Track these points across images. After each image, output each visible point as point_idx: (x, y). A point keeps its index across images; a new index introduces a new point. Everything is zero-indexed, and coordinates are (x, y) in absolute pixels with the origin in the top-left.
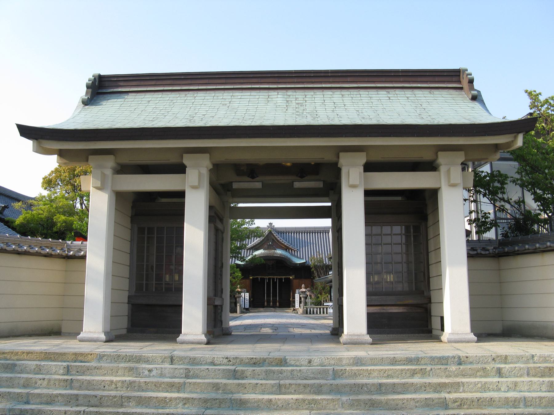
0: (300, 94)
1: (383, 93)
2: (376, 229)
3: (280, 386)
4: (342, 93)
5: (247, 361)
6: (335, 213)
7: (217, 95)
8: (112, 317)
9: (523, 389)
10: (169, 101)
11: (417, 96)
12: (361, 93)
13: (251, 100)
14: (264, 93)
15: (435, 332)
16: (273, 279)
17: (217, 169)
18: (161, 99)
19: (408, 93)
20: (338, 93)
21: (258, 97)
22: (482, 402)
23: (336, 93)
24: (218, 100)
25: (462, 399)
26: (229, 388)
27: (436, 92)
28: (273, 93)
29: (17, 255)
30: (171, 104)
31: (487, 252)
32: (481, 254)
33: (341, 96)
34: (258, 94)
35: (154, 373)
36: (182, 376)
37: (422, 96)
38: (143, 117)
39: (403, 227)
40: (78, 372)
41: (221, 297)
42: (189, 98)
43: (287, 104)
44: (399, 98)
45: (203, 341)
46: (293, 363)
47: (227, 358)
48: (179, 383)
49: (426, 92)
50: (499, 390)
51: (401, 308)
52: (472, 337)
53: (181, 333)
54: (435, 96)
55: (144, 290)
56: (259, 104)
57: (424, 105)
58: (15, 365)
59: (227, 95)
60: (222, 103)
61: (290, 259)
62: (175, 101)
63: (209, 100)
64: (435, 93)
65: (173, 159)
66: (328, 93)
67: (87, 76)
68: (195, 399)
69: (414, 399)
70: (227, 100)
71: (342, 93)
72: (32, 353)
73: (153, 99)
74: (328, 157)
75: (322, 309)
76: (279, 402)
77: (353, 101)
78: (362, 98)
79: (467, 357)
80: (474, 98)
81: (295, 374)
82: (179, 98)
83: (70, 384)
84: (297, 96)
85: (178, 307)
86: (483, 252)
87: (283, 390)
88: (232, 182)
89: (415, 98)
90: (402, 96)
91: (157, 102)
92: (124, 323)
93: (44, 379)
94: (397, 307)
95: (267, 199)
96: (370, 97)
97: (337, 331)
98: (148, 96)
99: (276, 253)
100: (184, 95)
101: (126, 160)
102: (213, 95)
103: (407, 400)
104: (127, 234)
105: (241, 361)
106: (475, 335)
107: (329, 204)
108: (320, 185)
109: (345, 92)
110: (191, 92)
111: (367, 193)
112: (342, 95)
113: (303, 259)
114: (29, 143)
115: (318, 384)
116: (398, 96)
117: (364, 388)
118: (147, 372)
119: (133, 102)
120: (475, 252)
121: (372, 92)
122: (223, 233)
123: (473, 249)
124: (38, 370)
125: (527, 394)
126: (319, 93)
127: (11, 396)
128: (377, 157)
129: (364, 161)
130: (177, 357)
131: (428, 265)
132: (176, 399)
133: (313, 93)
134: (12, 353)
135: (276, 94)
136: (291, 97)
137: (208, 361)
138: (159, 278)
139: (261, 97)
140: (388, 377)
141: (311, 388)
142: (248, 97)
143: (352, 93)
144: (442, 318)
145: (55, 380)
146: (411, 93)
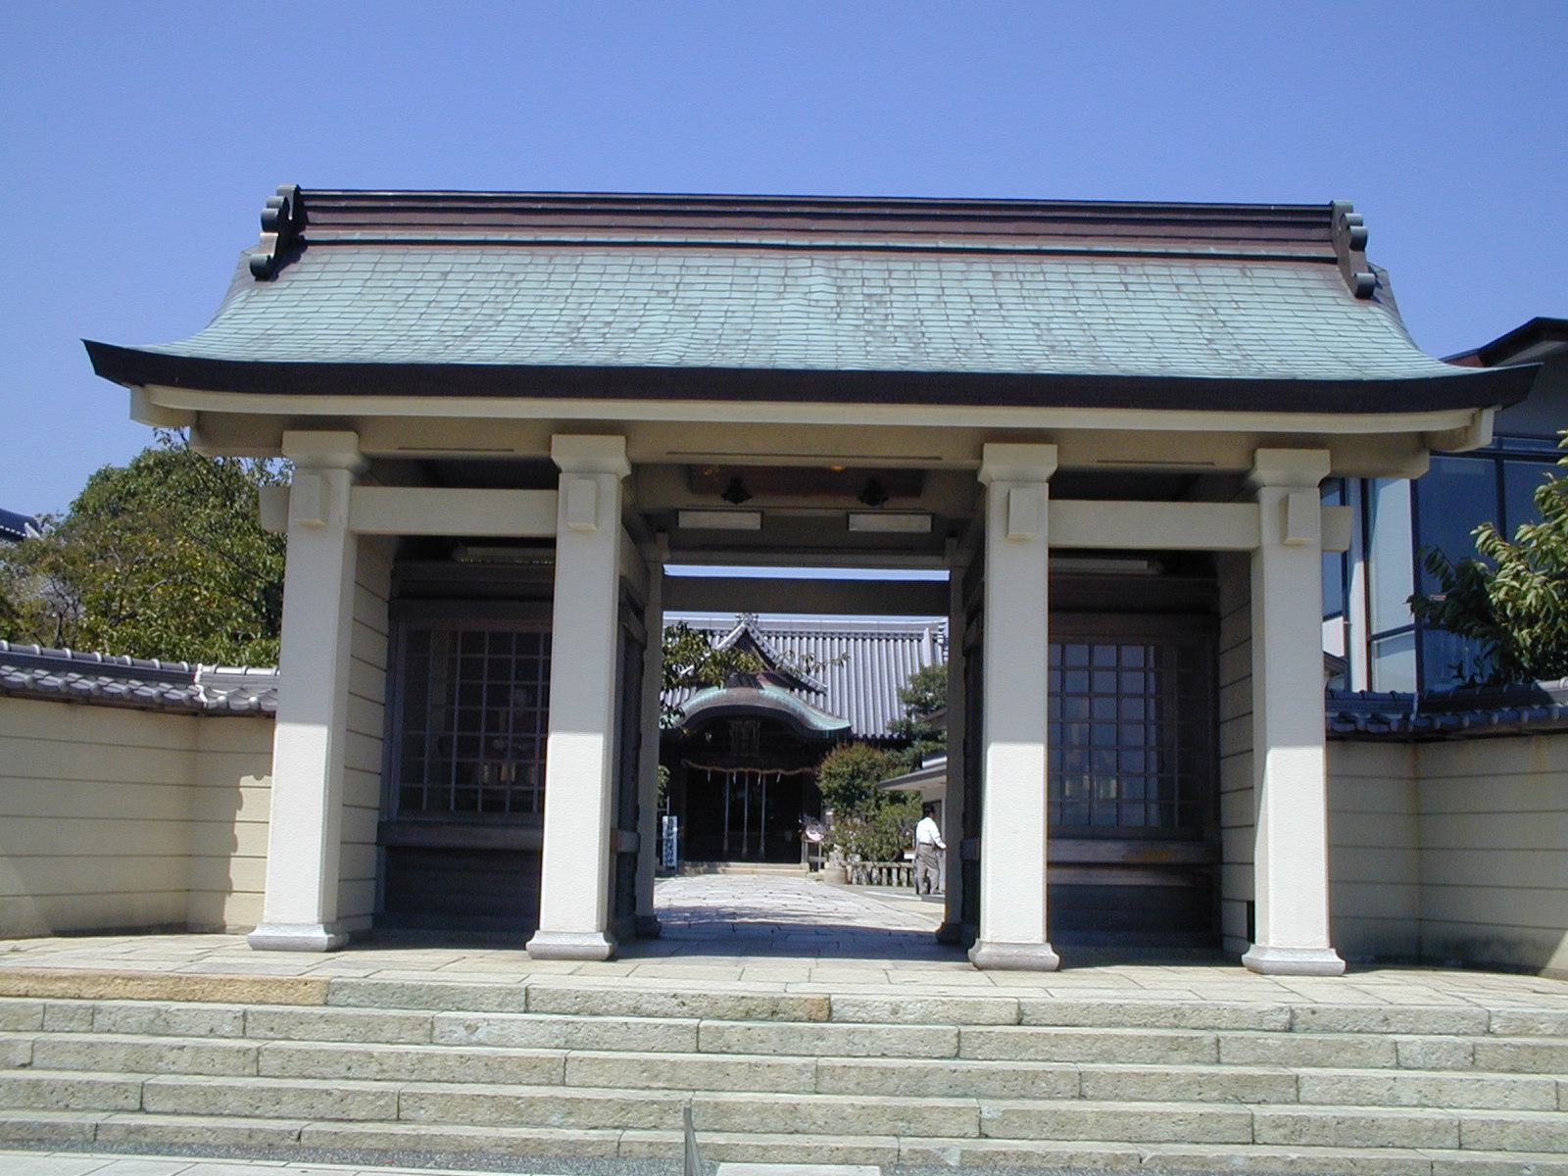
0: (872, 268)
1: (1108, 269)
2: (1077, 654)
3: (818, 1071)
4: (995, 268)
5: (730, 1004)
6: (965, 605)
7: (639, 261)
8: (342, 882)
9: (1459, 1100)
10: (502, 277)
11: (1204, 281)
12: (1046, 268)
13: (737, 280)
14: (773, 262)
15: (1229, 945)
16: (753, 777)
17: (639, 475)
18: (480, 268)
19: (1181, 271)
20: (981, 267)
21: (755, 272)
22: (1350, 1127)
23: (975, 267)
24: (644, 278)
25: (1297, 1120)
26: (684, 1073)
27: (1260, 271)
28: (801, 261)
29: (66, 706)
30: (510, 285)
31: (1385, 728)
32: (1366, 732)
33: (989, 276)
34: (757, 263)
35: (480, 1035)
36: (557, 1041)
37: (1220, 281)
38: (435, 325)
39: (1152, 649)
40: (272, 1029)
41: (634, 829)
42: (560, 269)
43: (840, 298)
44: (1154, 287)
45: (600, 950)
46: (849, 1012)
47: (675, 996)
48: (551, 1060)
49: (1231, 270)
50: (1394, 1102)
51: (1137, 874)
52: (1333, 959)
53: (538, 928)
54: (1257, 282)
55: (424, 808)
56: (760, 295)
57: (1225, 312)
58: (95, 1011)
59: (669, 263)
60: (657, 287)
61: (802, 716)
62: (521, 277)
63: (618, 278)
64: (1257, 273)
65: (525, 449)
66: (954, 265)
67: (268, 198)
68: (597, 1101)
69: (1170, 1115)
70: (670, 279)
71: (995, 268)
72: (139, 978)
73: (457, 268)
74: (955, 457)
75: (895, 871)
76: (818, 1114)
77: (1025, 293)
78: (1050, 286)
79: (1314, 1012)
80: (1365, 293)
81: (856, 1040)
82: (530, 269)
83: (254, 1062)
84: (866, 274)
85: (532, 857)
86: (1372, 728)
87: (827, 1082)
88: (676, 511)
89: (1198, 290)
90: (1163, 280)
91: (470, 276)
92: (367, 898)
93: (182, 1048)
94: (1125, 873)
95: (776, 557)
96: (1073, 283)
97: (957, 938)
98: (444, 258)
99: (760, 698)
100: (544, 260)
101: (387, 447)
102: (629, 261)
103: (1153, 1116)
104: (377, 649)
105: (714, 1009)
106: (1340, 956)
107: (943, 575)
108: (920, 524)
109: (1003, 265)
110: (564, 250)
111: (1055, 553)
112: (995, 274)
113: (840, 717)
114: (119, 395)
115: (919, 1070)
116: (1152, 280)
117: (1037, 1081)
118: (461, 1032)
119: (399, 276)
120: (1350, 727)
121: (1079, 268)
122: (644, 647)
123: (1345, 718)
124: (160, 1025)
125: (1467, 1114)
126: (928, 266)
127: (96, 1091)
128: (1085, 459)
129: (1051, 469)
130: (541, 990)
131: (1218, 758)
132: (545, 1100)
133: (910, 266)
134: (84, 978)
135: (808, 263)
136: (850, 274)
137: (625, 1003)
138: (466, 774)
139: (764, 272)
140: (1109, 1057)
141: (901, 1080)
142: (729, 271)
143: (1021, 268)
144: (1251, 905)
145: (215, 1050)
146: (1187, 272)
